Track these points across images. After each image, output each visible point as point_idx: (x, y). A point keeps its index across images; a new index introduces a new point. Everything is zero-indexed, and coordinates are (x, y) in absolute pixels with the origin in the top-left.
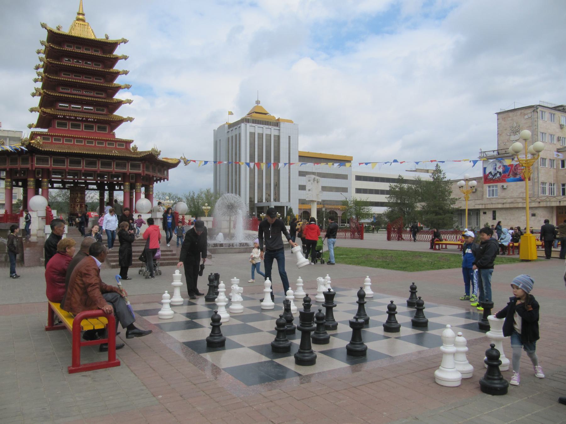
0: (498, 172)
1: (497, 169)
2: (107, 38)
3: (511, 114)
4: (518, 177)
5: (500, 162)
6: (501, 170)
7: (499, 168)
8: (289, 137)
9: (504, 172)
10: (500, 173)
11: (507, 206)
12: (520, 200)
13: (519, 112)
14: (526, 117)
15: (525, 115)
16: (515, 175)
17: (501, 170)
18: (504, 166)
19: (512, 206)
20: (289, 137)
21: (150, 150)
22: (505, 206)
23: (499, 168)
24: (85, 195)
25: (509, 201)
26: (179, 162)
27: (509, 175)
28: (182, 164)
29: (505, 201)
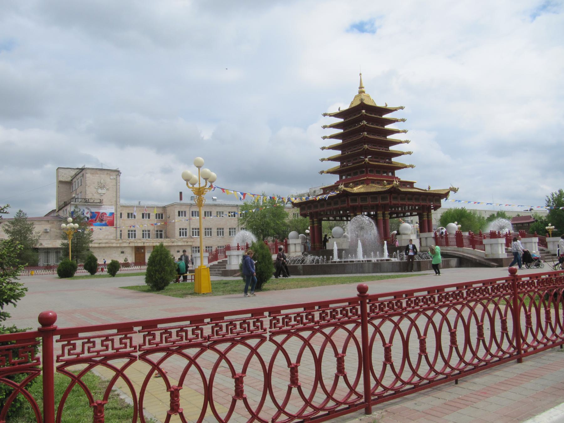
0: (85, 217)
1: (85, 214)
2: (386, 105)
3: (99, 172)
4: (104, 223)
5: (88, 209)
6: (89, 216)
7: (87, 213)
8: (181, 193)
9: (91, 217)
10: (88, 218)
11: (104, 245)
12: (114, 241)
13: (106, 172)
14: (112, 177)
15: (110, 175)
16: (102, 220)
17: (89, 216)
18: (92, 213)
19: (107, 245)
20: (181, 193)
21: (460, 208)
22: (101, 245)
23: (87, 213)
24: (298, 207)
25: (105, 241)
26: (448, 192)
27: (96, 220)
28: (451, 193)
29: (101, 241)
